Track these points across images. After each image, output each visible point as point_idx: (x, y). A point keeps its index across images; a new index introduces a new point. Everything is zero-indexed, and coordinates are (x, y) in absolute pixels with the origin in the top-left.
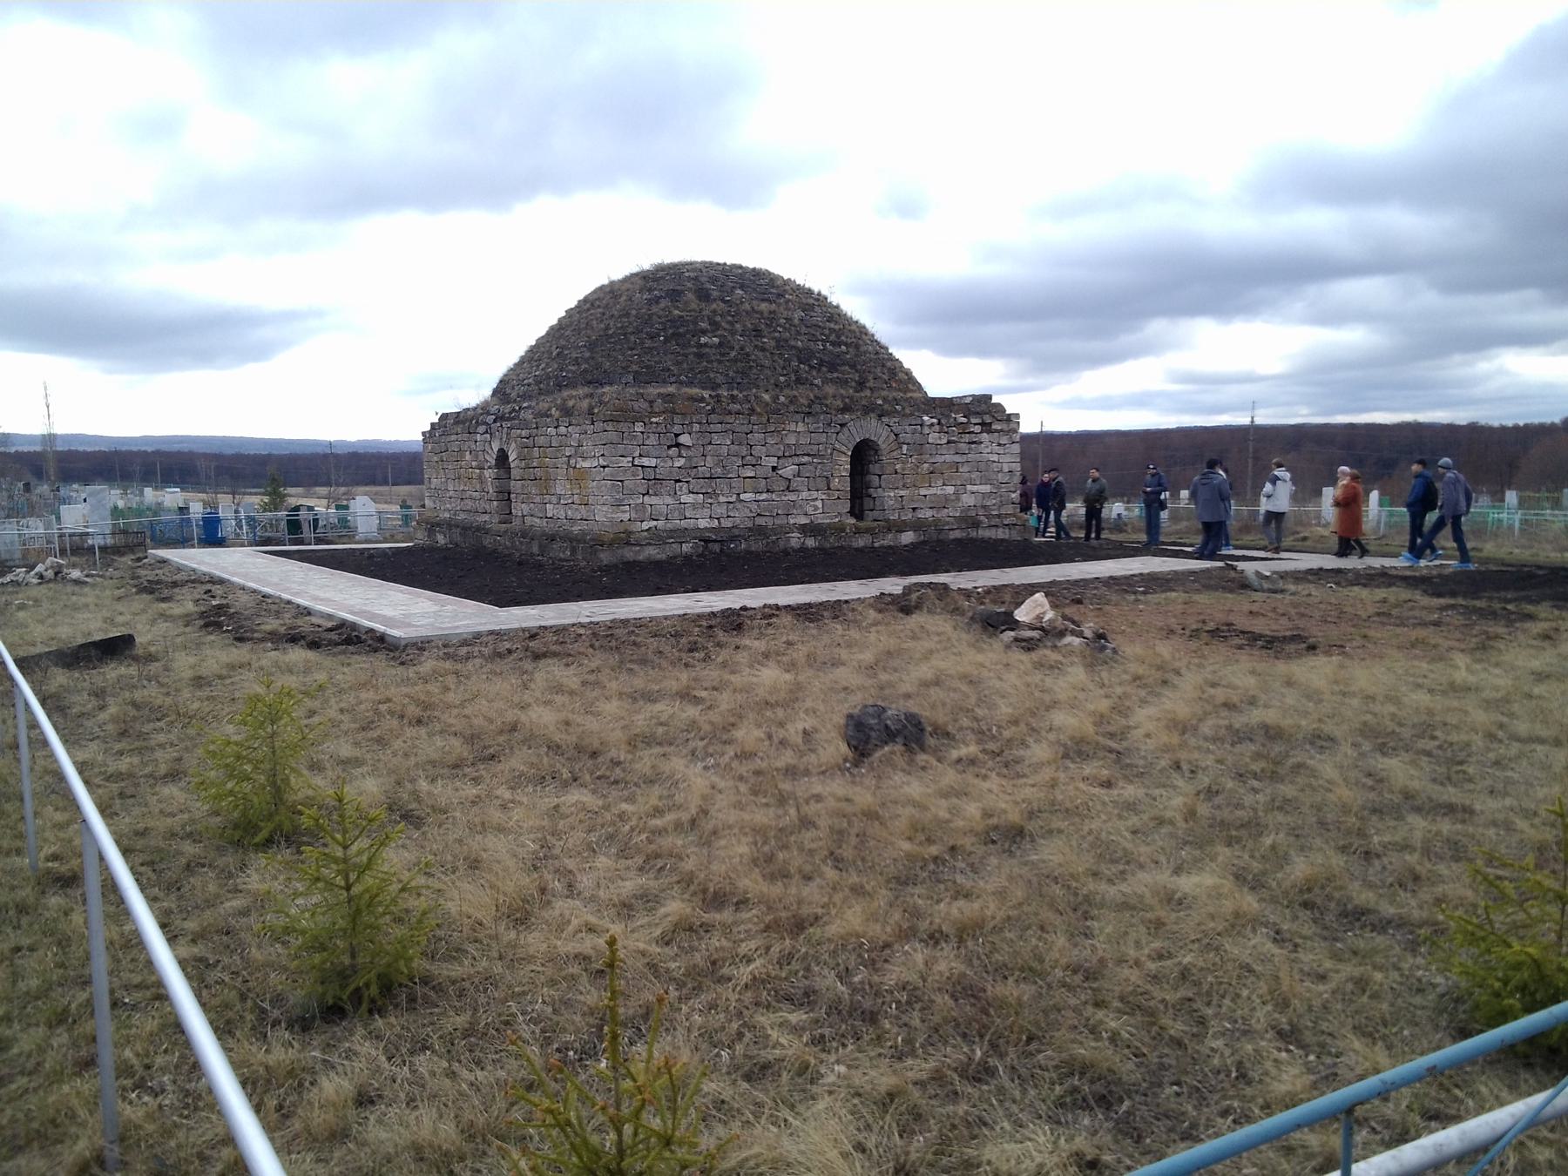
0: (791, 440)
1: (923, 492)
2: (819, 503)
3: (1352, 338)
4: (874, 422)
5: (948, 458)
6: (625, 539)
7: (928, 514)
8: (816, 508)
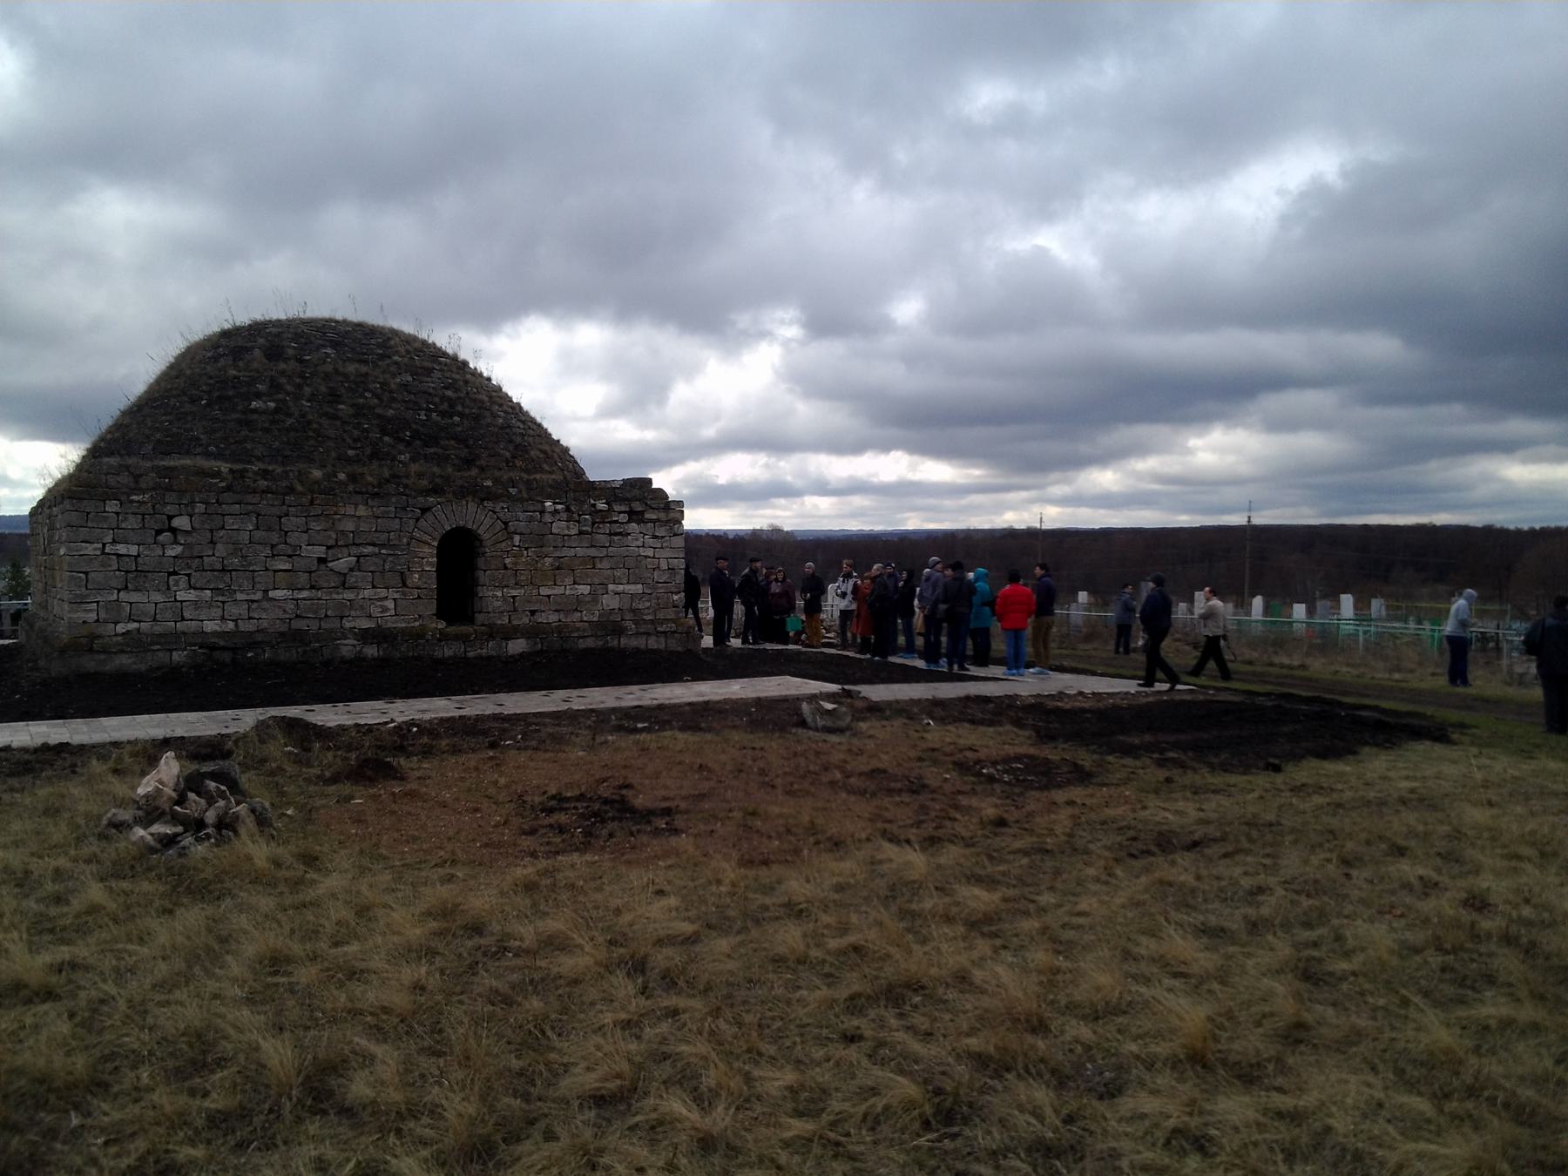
0: (349, 526)
1: (544, 591)
3: (1312, 444)
4: (472, 507)
5: (580, 552)
6: (88, 643)
7: (553, 618)
8: (385, 609)
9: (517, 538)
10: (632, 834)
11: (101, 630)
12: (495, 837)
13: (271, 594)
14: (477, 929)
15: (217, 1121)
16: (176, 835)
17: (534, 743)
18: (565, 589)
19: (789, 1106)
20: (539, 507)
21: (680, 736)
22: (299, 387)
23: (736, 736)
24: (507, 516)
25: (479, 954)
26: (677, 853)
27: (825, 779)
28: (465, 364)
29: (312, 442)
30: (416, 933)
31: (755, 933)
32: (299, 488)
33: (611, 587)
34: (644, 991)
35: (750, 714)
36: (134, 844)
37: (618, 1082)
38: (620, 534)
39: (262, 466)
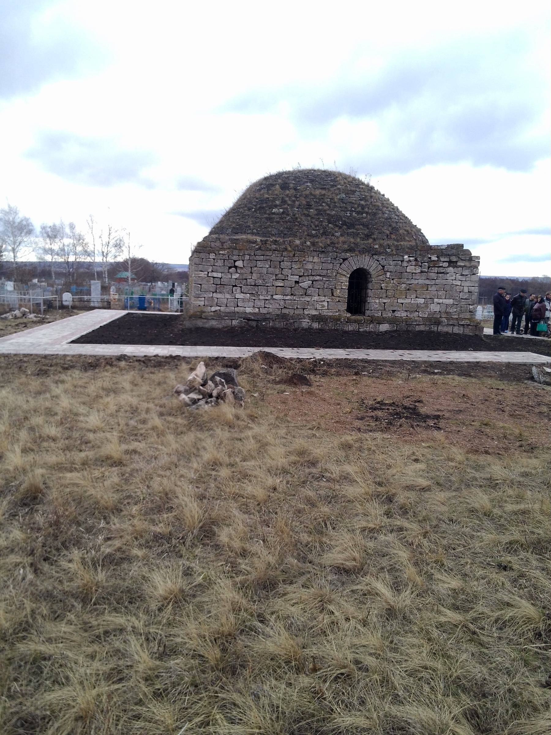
0: (310, 266)
1: (400, 301)
2: (326, 304)
4: (367, 258)
5: (420, 282)
6: (200, 315)
7: (404, 314)
8: (323, 306)
9: (388, 274)
10: (412, 427)
11: (205, 309)
12: (342, 419)
13: (274, 297)
14: (313, 464)
15: (158, 538)
16: (199, 400)
17: (377, 375)
18: (410, 300)
19: (450, 601)
20: (401, 259)
21: (457, 378)
22: (294, 201)
23: (489, 381)
24: (383, 262)
25: (310, 477)
26: (434, 440)
27: (537, 410)
28: (372, 188)
29: (297, 227)
30: (282, 462)
31: (465, 492)
32: (289, 249)
33: (436, 300)
34: (388, 514)
35: (501, 371)
36: (180, 401)
37: (354, 563)
38: (443, 273)
39: (274, 238)
